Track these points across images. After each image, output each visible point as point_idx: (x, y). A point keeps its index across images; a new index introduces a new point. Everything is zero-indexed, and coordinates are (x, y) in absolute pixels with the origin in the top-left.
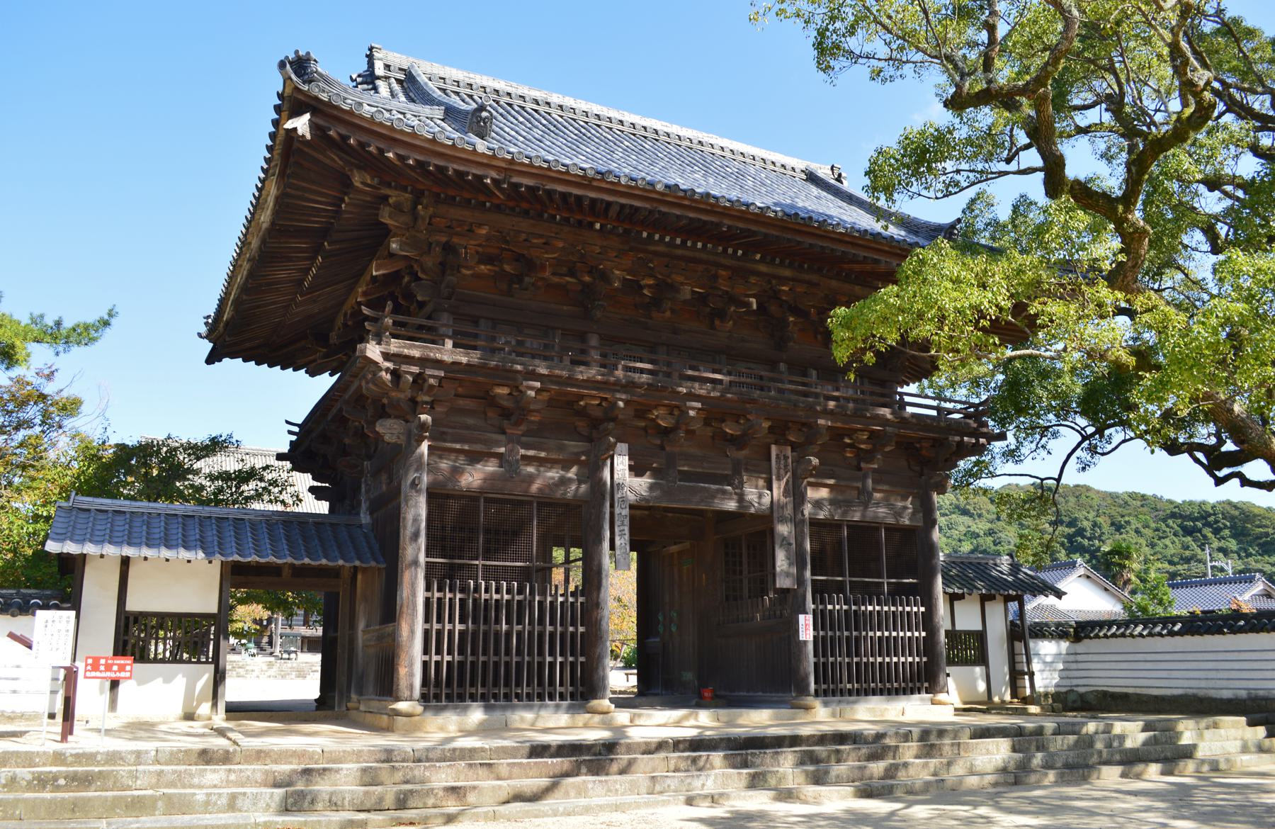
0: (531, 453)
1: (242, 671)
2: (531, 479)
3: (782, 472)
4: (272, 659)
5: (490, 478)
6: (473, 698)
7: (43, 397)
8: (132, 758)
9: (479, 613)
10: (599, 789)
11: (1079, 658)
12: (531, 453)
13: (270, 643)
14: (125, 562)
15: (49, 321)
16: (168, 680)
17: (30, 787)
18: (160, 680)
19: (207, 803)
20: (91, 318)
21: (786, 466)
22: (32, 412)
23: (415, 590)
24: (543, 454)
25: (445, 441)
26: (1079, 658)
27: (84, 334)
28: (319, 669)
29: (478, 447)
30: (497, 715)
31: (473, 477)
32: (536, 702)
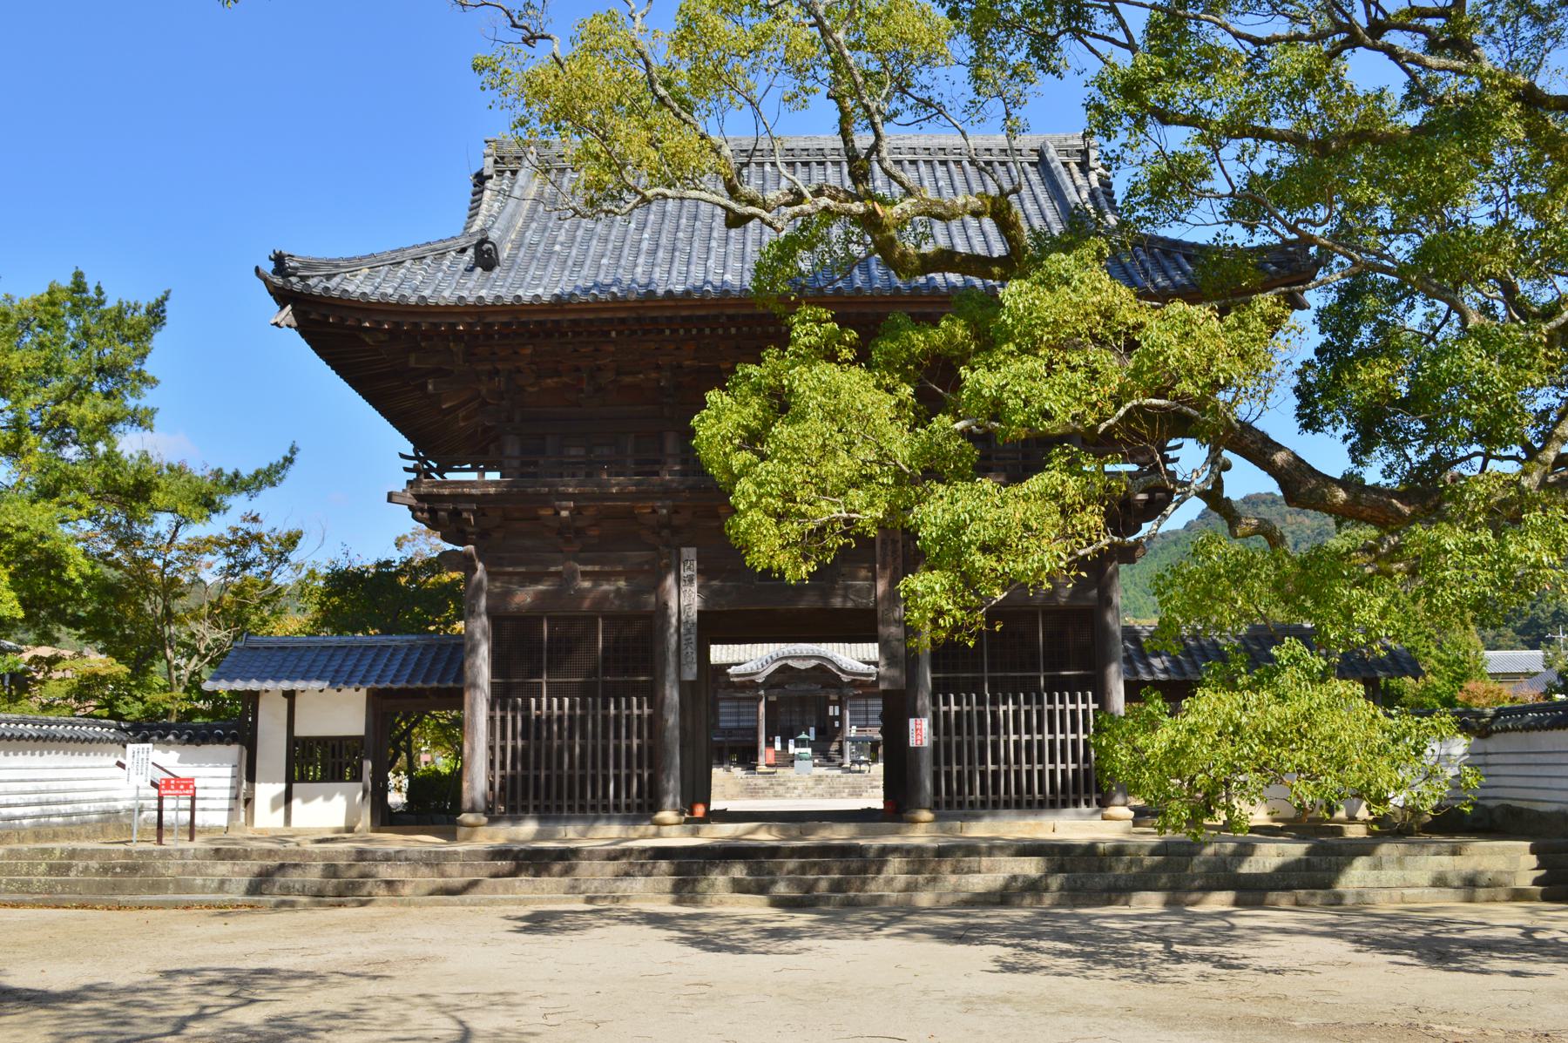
0: (589, 568)
1: (781, 789)
2: (582, 594)
3: (889, 559)
4: (839, 772)
5: (541, 596)
6: (525, 809)
7: (258, 538)
8: (178, 855)
9: (533, 729)
10: (526, 887)
11: (1490, 759)
12: (589, 568)
13: (841, 752)
14: (290, 695)
15: (229, 471)
16: (328, 798)
17: (97, 873)
18: (320, 799)
19: (204, 886)
20: (277, 458)
21: (894, 552)
22: (254, 552)
23: (479, 709)
24: (597, 568)
25: (501, 565)
26: (1490, 759)
27: (268, 477)
28: (881, 783)
29: (536, 568)
30: (549, 827)
31: (524, 597)
32: (590, 814)
